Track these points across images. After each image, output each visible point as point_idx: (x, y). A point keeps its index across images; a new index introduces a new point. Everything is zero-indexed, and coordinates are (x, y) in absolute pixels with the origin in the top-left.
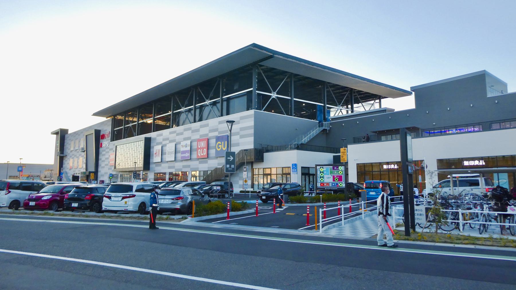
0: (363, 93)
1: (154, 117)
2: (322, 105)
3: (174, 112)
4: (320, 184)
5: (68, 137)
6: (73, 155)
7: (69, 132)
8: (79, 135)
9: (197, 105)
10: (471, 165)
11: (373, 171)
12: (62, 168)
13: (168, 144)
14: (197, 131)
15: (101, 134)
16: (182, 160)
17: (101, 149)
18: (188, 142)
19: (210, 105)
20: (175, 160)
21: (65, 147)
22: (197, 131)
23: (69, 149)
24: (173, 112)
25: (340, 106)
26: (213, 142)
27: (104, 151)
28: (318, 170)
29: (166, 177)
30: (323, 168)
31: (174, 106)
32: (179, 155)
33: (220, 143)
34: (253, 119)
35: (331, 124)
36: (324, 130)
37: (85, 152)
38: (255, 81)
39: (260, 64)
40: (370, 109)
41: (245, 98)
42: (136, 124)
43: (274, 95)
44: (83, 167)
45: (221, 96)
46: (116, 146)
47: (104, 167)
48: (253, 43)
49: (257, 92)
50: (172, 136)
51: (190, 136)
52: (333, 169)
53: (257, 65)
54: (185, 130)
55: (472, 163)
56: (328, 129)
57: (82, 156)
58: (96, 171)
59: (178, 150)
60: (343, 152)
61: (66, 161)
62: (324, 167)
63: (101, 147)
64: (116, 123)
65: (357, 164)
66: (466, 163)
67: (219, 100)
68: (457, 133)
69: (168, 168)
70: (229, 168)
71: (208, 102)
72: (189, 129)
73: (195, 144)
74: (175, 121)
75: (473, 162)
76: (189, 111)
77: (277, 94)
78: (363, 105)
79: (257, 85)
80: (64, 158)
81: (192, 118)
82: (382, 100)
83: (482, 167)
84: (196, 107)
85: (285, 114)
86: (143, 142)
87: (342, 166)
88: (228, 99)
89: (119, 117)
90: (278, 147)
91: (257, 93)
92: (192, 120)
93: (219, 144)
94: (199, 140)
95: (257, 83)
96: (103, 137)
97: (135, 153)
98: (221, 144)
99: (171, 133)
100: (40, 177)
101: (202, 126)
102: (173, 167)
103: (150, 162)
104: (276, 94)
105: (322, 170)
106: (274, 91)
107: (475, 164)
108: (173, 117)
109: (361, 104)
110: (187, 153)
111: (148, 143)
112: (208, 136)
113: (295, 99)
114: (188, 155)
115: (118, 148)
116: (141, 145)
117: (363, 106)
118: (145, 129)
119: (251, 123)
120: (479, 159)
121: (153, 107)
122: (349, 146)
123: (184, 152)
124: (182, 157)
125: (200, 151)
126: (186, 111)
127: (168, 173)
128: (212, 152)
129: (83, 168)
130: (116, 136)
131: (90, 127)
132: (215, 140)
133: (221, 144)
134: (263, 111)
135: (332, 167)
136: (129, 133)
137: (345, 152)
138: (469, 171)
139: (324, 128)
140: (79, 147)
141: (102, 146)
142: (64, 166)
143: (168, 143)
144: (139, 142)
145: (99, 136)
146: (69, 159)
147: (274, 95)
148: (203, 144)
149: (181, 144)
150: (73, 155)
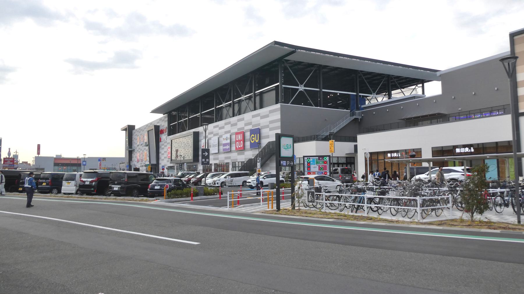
0: (403, 78)
1: (201, 112)
2: (355, 94)
3: (217, 107)
4: (307, 173)
5: (135, 133)
6: (139, 149)
7: (136, 128)
8: (143, 131)
9: (235, 100)
10: (462, 152)
11: (300, 163)
12: (131, 161)
13: (213, 137)
14: (235, 124)
15: (160, 130)
16: (224, 152)
17: (161, 144)
18: (228, 135)
19: (246, 99)
20: (218, 152)
21: (133, 142)
22: (235, 124)
23: (136, 144)
24: (170, 125)
25: (375, 94)
26: (248, 134)
27: (163, 145)
28: (306, 160)
29: (212, 168)
30: (310, 159)
31: (216, 101)
32: (221, 148)
33: (254, 136)
34: (279, 112)
35: (362, 113)
36: (356, 119)
37: (148, 146)
38: (281, 76)
39: (287, 58)
40: (382, 100)
41: (274, 92)
42: (231, 103)
43: (301, 88)
44: (147, 160)
45: (232, 100)
46: (172, 140)
47: (164, 159)
48: (274, 41)
49: (283, 86)
50: (216, 130)
51: (230, 130)
52: (319, 159)
53: (283, 60)
54: (226, 124)
55: (463, 150)
56: (360, 117)
57: (146, 150)
58: (157, 163)
59: (220, 143)
60: (331, 144)
61: (134, 154)
62: (311, 158)
63: (161, 141)
64: (171, 118)
65: (432, 148)
66: (458, 150)
67: (252, 95)
68: (480, 118)
69: (214, 160)
70: (204, 162)
71: (242, 97)
72: (229, 123)
73: (234, 137)
74: (219, 116)
75: (464, 149)
76: (230, 105)
77: (304, 87)
78: (403, 91)
79: (283, 80)
80: (133, 152)
81: (251, 105)
82: (425, 84)
83: (471, 153)
84: (235, 102)
85: (314, 105)
86: (192, 136)
87: (327, 157)
88: (261, 94)
89: (174, 113)
90: (299, 138)
91: (284, 87)
92: (253, 108)
93: (253, 137)
94: (237, 134)
95: (283, 78)
96: (162, 132)
97: (187, 146)
98: (255, 137)
99: (215, 127)
100: (116, 169)
101: (239, 120)
102: (217, 159)
103: (199, 155)
104: (303, 86)
105: (309, 160)
106: (302, 84)
107: (465, 151)
108: (216, 112)
109: (400, 90)
110: (227, 146)
111: (196, 135)
112: (244, 129)
113: (323, 90)
114: (228, 147)
115: (173, 142)
116: (190, 140)
117: (402, 92)
118: (194, 124)
119: (277, 116)
120: (469, 146)
121: (199, 103)
122: (360, 137)
123: (225, 145)
124: (224, 150)
125: (256, 140)
126: (246, 99)
127: (214, 164)
128: (248, 144)
129: (147, 161)
130: (172, 131)
131: (151, 123)
132: (249, 133)
133: (255, 137)
134: (292, 103)
135: (318, 157)
136: (181, 128)
137: (332, 144)
138: (488, 157)
139: (354, 117)
140: (143, 141)
141: (161, 141)
142: (133, 159)
143: (224, 134)
144: (189, 136)
145: (158, 131)
146: (136, 153)
147: (301, 88)
148: (240, 137)
149: (223, 138)
150: (139, 149)
